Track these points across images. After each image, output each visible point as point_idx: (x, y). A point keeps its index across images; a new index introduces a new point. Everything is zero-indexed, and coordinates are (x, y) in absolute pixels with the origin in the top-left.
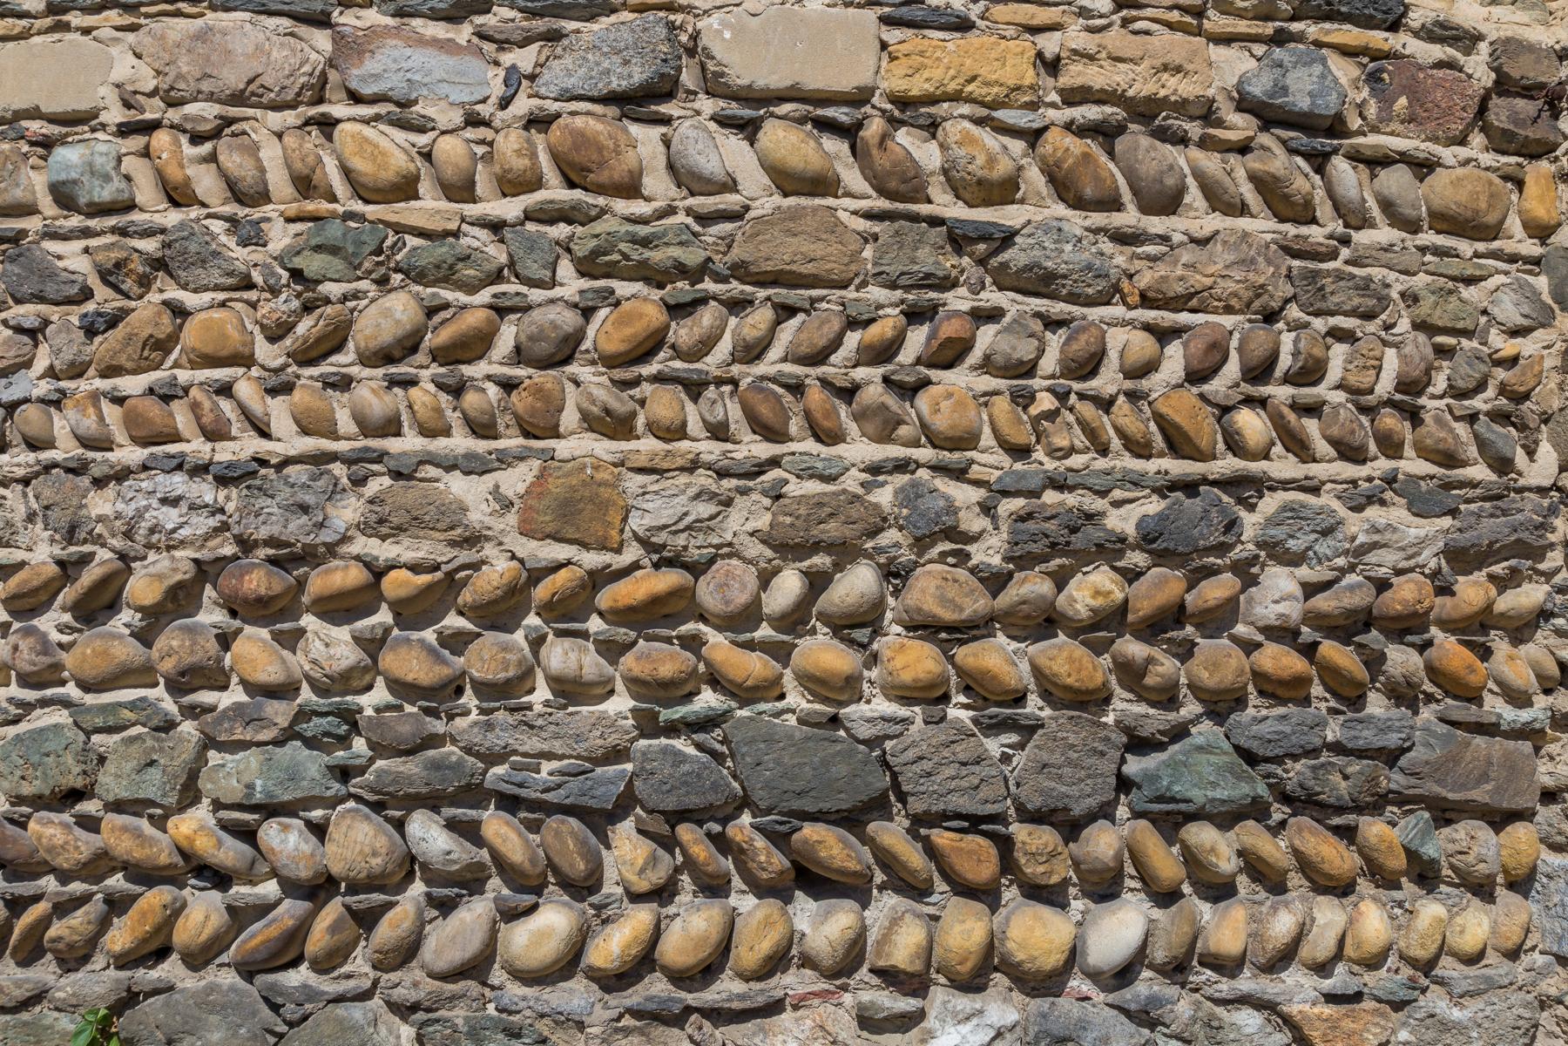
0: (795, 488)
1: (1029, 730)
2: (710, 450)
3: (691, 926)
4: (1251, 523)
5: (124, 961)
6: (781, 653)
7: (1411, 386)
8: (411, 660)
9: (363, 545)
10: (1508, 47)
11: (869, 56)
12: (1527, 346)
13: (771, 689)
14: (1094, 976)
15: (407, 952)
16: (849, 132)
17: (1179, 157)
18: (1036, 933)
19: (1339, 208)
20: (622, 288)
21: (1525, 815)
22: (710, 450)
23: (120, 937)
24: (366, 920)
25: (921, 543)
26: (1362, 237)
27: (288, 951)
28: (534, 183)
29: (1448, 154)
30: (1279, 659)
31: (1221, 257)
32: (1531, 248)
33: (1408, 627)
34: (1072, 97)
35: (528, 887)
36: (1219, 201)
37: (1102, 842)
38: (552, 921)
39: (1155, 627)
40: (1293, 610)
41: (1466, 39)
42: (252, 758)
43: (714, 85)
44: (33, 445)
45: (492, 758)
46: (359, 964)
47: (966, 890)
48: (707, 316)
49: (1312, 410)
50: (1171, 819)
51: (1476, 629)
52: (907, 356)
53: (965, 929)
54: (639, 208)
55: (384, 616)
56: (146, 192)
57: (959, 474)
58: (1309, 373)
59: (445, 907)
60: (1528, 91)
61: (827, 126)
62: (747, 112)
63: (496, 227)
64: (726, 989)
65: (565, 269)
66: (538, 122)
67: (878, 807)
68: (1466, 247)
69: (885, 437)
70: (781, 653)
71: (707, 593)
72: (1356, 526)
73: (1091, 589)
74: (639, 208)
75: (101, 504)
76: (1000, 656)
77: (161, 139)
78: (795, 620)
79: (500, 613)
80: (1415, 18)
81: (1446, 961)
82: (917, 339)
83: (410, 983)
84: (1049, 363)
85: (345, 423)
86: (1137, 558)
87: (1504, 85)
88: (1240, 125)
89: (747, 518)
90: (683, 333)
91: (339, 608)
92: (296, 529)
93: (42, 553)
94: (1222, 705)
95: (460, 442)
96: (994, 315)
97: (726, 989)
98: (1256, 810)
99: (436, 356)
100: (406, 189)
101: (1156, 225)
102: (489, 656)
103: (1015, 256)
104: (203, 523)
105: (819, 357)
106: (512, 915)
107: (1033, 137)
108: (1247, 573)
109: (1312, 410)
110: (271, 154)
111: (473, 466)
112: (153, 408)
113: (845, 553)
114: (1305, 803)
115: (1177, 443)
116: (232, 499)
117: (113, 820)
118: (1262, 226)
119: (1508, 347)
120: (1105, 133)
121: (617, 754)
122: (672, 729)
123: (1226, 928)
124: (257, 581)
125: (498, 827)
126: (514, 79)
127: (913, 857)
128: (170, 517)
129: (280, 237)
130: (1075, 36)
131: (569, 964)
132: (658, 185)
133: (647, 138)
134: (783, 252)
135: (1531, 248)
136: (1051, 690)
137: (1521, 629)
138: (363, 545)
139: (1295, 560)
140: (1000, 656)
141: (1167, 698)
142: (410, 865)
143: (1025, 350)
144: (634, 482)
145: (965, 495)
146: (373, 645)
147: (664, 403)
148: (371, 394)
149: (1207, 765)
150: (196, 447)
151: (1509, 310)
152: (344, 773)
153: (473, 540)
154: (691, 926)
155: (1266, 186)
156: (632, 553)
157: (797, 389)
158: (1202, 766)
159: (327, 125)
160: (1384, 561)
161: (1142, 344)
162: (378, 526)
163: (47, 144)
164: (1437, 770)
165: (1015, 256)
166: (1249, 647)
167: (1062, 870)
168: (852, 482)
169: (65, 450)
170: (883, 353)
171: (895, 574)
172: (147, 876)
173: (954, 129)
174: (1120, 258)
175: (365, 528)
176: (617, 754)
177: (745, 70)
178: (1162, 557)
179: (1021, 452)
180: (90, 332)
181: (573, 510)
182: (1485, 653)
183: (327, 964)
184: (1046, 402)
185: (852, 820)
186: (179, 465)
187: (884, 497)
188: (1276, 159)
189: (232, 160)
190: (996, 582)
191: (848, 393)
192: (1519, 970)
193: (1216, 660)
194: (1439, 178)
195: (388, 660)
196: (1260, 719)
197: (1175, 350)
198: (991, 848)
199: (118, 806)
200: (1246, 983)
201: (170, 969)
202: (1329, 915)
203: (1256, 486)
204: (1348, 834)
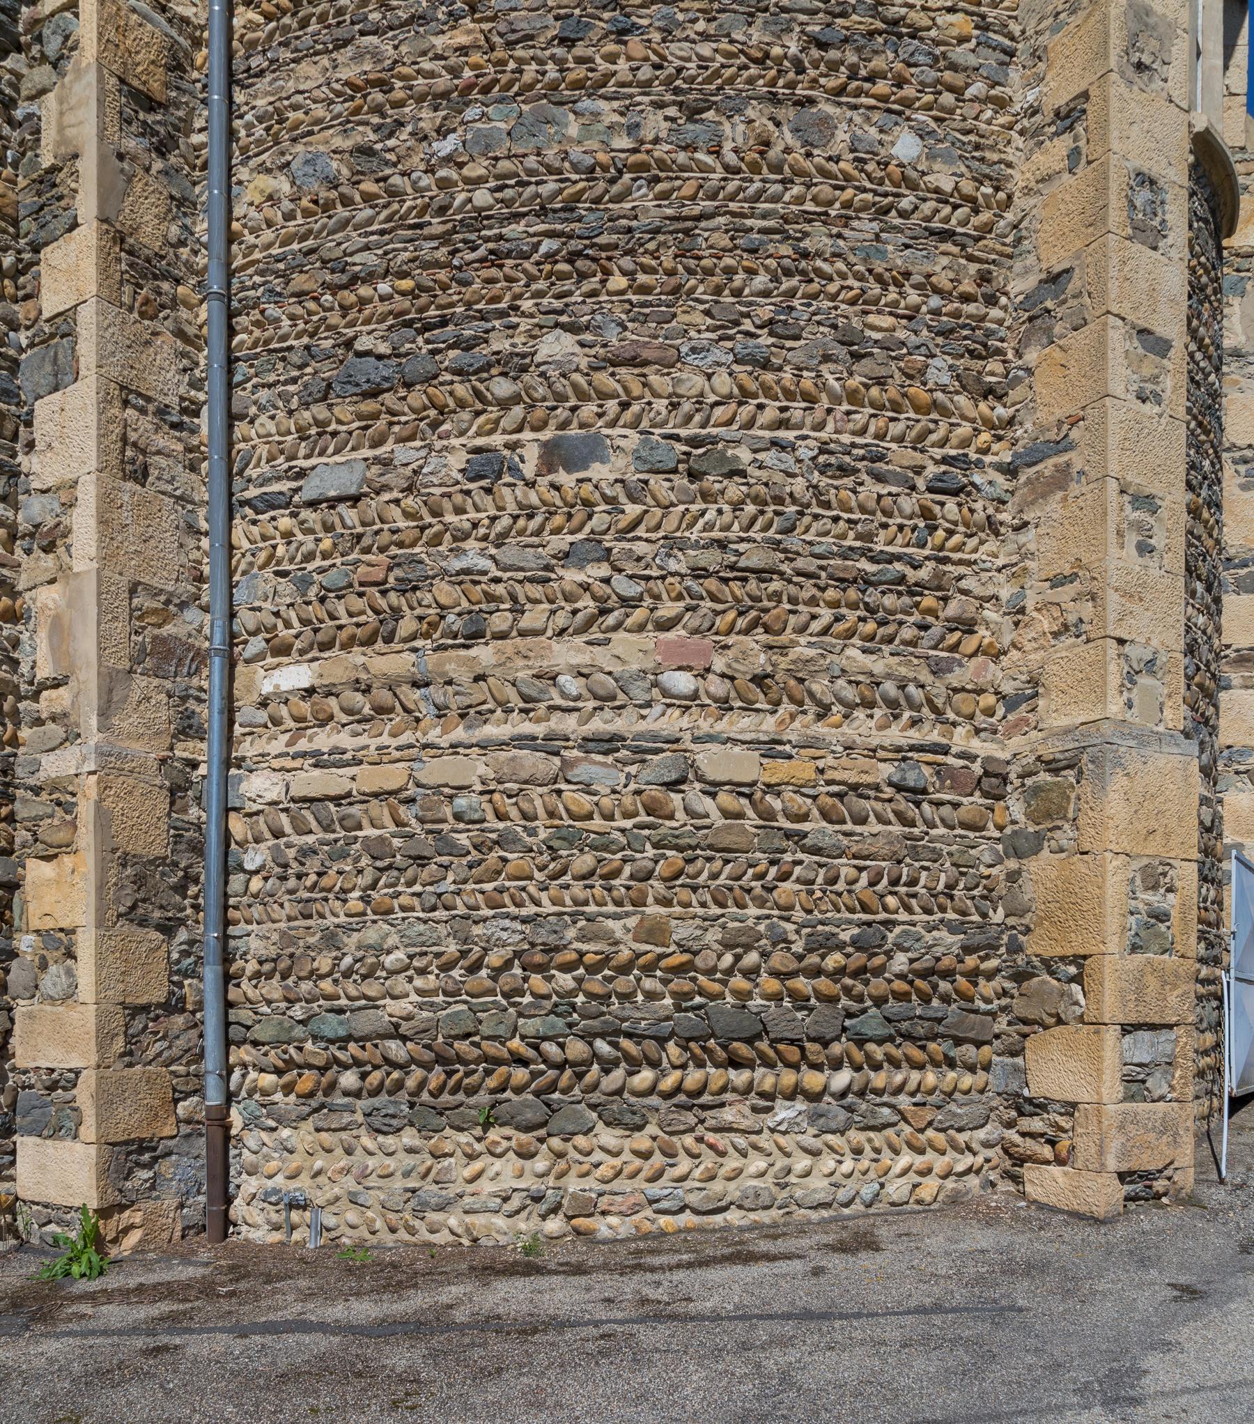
0: (731, 925)
1: (811, 1010)
2: (700, 911)
3: (694, 1077)
4: (891, 937)
5: (493, 1091)
6: (724, 983)
7: (951, 886)
8: (595, 984)
9: (576, 945)
10: (988, 760)
11: (757, 768)
12: (994, 871)
13: (721, 996)
14: (832, 1095)
15: (595, 1087)
16: (749, 796)
17: (867, 804)
18: (813, 1080)
19: (925, 821)
20: (669, 853)
21: (989, 1043)
22: (700, 911)
23: (492, 1082)
24: (580, 1076)
25: (774, 944)
26: (933, 832)
27: (552, 1087)
28: (636, 814)
29: (965, 800)
30: (900, 986)
31: (881, 841)
32: (997, 834)
33: (948, 974)
34: (829, 783)
35: (634, 1066)
36: (881, 820)
37: (836, 1048)
38: (646, 1076)
39: (855, 974)
40: (905, 968)
41: (972, 758)
42: (537, 1020)
43: (700, 779)
44: (447, 908)
45: (624, 1020)
46: (576, 1091)
47: (788, 1065)
48: (699, 863)
49: (914, 896)
50: (860, 1042)
51: (973, 975)
52: (770, 877)
53: (788, 1078)
54: (674, 824)
55: (581, 971)
56: (490, 815)
57: (788, 919)
58: (913, 882)
59: (607, 1072)
60: (996, 776)
61: (740, 794)
63: (623, 831)
64: (706, 1098)
65: (648, 846)
66: (638, 792)
67: (758, 1037)
68: (971, 835)
69: (761, 907)
70: (724, 983)
71: (699, 961)
72: (929, 938)
73: (834, 960)
74: (674, 824)
75: (477, 930)
76: (802, 984)
77: (496, 796)
78: (729, 972)
79: (624, 969)
80: (954, 750)
82: (773, 871)
83: (595, 1097)
84: (820, 880)
85: (568, 901)
86: (850, 950)
87: (987, 774)
88: (889, 792)
89: (713, 936)
90: (690, 869)
91: (566, 968)
92: (552, 939)
93: (452, 948)
94: (879, 1001)
95: (611, 908)
96: (800, 862)
97: (706, 1098)
98: (891, 1039)
99: (603, 877)
100: (589, 817)
101: (858, 829)
102: (623, 983)
103: (808, 841)
104: (518, 937)
105: (739, 878)
106: (631, 1074)
107: (814, 798)
108: (889, 955)
109: (914, 896)
110: (538, 803)
111: (616, 917)
112: (496, 895)
113: (748, 948)
114: (908, 1037)
115: (865, 908)
116: (527, 928)
117: (484, 1044)
118: (897, 829)
119: (986, 872)
120: (840, 796)
121: (668, 1018)
122: (686, 1010)
124: (539, 958)
125: (625, 1043)
126: (628, 776)
127: (771, 1053)
128: (504, 935)
129: (543, 834)
130: (830, 761)
131: (651, 1091)
132: (680, 815)
133: (676, 798)
134: (727, 841)
135: (997, 834)
136: (820, 996)
137: (990, 976)
138: (576, 945)
139: (907, 950)
140: (802, 984)
141: (860, 999)
142: (595, 1055)
143: (811, 876)
144: (674, 923)
145: (790, 927)
146: (580, 981)
147: (685, 895)
148: (578, 889)
149: (873, 1022)
150: (512, 910)
151: (987, 858)
152: (570, 1025)
153: (616, 943)
154: (694, 1077)
155: (898, 814)
156: (673, 948)
157: (731, 889)
158: (872, 1022)
159: (559, 792)
160: (938, 951)
161: (853, 873)
162: (582, 938)
163: (451, 797)
164: (955, 1026)
165: (808, 841)
166: (889, 981)
167: (822, 1059)
168: (750, 922)
169: (461, 910)
170: (760, 877)
171: (765, 955)
172: (499, 1062)
173: (788, 795)
174: (845, 841)
175: (578, 939)
176: (668, 1018)
177: (711, 776)
178: (858, 949)
179: (809, 912)
180: (470, 867)
181: (653, 933)
182: (976, 984)
183: (565, 1091)
184: (818, 894)
185: (749, 1041)
186: (507, 916)
187: (761, 928)
188: (903, 805)
189: (525, 806)
190: (800, 958)
191: (749, 891)
192: (984, 1098)
193: (878, 986)
194: (962, 809)
195: (586, 986)
196: (892, 1006)
197: (864, 874)
198: (799, 1051)
199: (488, 1038)
200: (885, 1098)
201: (508, 1094)
202: (915, 1076)
203: (894, 923)
204: (923, 1048)
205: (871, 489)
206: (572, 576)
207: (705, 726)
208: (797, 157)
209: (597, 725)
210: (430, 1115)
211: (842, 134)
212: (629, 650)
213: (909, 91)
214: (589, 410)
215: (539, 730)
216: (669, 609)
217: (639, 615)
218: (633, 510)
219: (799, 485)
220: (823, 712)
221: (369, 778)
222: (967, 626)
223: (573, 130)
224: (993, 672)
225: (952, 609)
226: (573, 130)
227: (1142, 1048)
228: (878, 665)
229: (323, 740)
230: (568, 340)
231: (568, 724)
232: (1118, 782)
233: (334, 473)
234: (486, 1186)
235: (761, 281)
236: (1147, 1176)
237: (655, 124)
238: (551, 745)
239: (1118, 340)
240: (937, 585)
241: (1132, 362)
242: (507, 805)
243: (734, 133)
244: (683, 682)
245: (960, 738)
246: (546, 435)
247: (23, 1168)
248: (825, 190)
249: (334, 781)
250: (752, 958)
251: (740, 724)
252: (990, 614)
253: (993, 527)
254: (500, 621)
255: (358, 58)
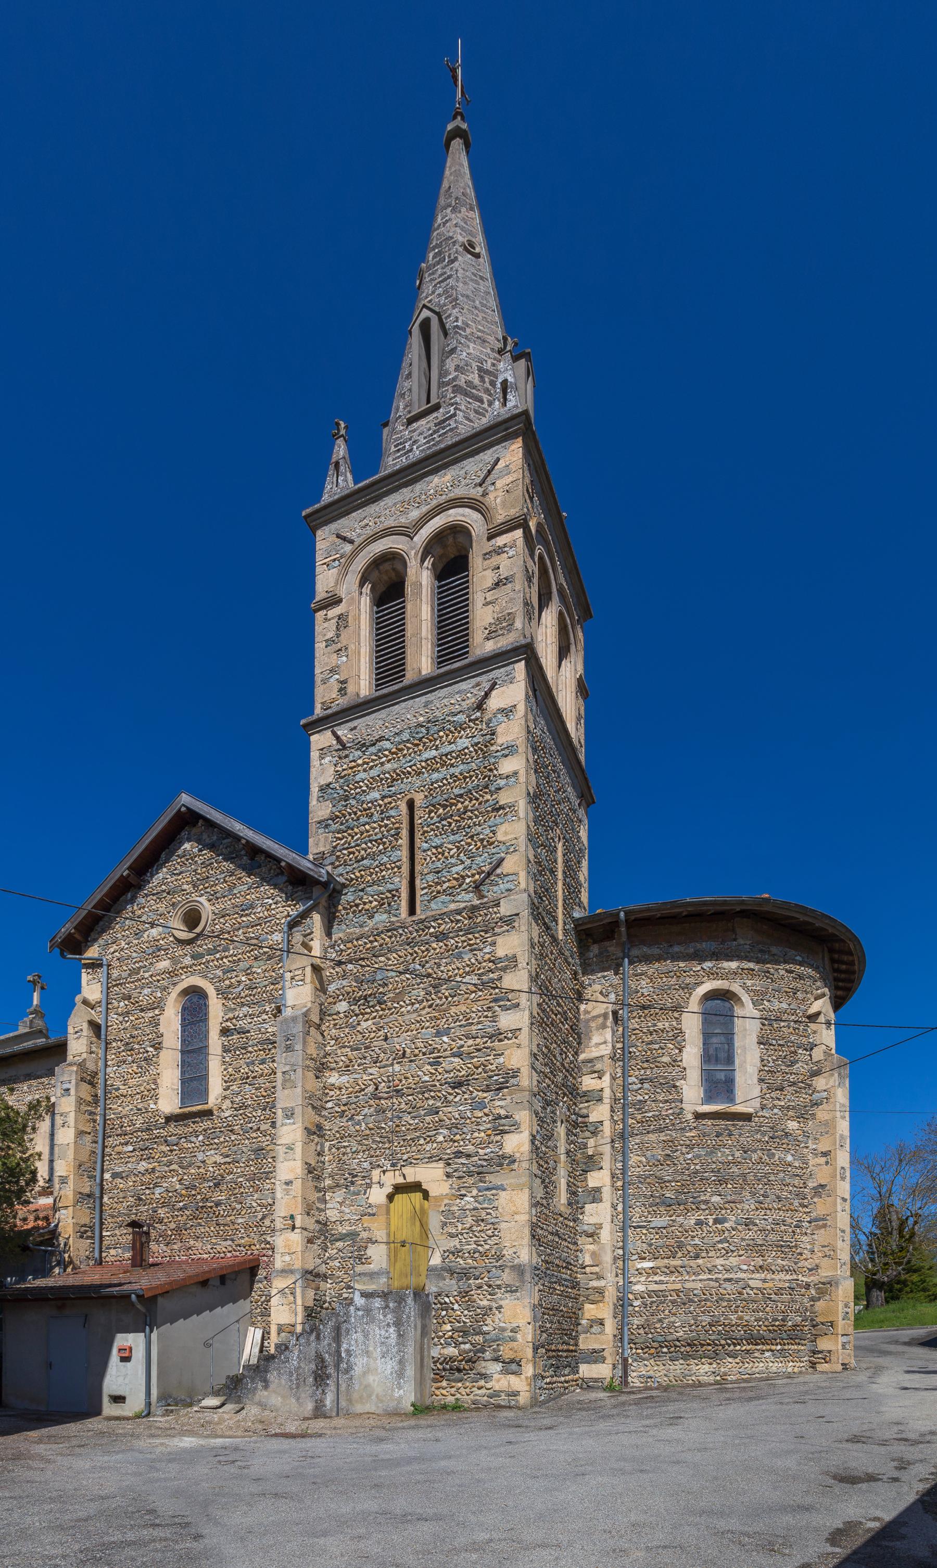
3: (749, 1347)
18: (773, 1347)
35: (735, 1345)
53: (768, 1347)
62: (752, 1289)
73: (777, 1323)
81: (501, 516)
89: (753, 1318)
93: (693, 1322)
123: (786, 1347)
148: (723, 1309)
154: (749, 1347)
158: (784, 1336)
181: (741, 1318)
193: (785, 1328)
205: (783, 1228)
206: (720, 1246)
207: (750, 1276)
208: (768, 1161)
209: (726, 1276)
210: (686, 1357)
211: (777, 1157)
212: (733, 1261)
213: (790, 1147)
214: (723, 1212)
215: (714, 1277)
216: (741, 1252)
217: (735, 1254)
218: (734, 1233)
219: (769, 1227)
220: (774, 1273)
221: (670, 1287)
222: (801, 1254)
223: (719, 1155)
224: (806, 1264)
225: (798, 1251)
226: (719, 1155)
227: (845, 1339)
228: (784, 1263)
229: (657, 1278)
230: (719, 1198)
231: (720, 1276)
232: (840, 1287)
233: (658, 1222)
234: (701, 1371)
235: (760, 1186)
236: (845, 1365)
237: (737, 1154)
238: (717, 1280)
239: (839, 1201)
240: (796, 1246)
241: (841, 1204)
242: (707, 1293)
243: (755, 1157)
244: (745, 1267)
245: (800, 1277)
246: (714, 1217)
247: (581, 1371)
248: (773, 1167)
249: (663, 1287)
250: (761, 1323)
251: (757, 1276)
252: (805, 1252)
253: (806, 1234)
254: (704, 1255)
255: (666, 1135)
